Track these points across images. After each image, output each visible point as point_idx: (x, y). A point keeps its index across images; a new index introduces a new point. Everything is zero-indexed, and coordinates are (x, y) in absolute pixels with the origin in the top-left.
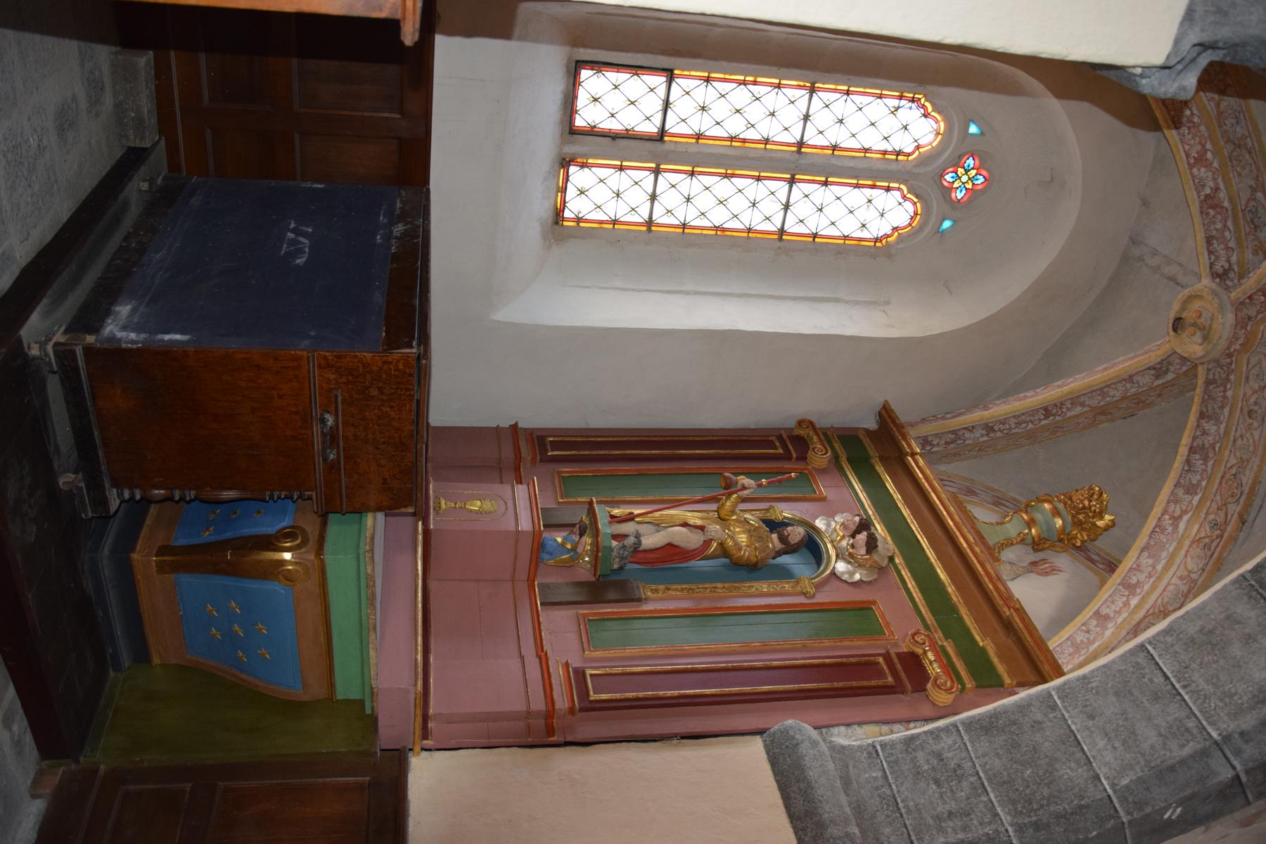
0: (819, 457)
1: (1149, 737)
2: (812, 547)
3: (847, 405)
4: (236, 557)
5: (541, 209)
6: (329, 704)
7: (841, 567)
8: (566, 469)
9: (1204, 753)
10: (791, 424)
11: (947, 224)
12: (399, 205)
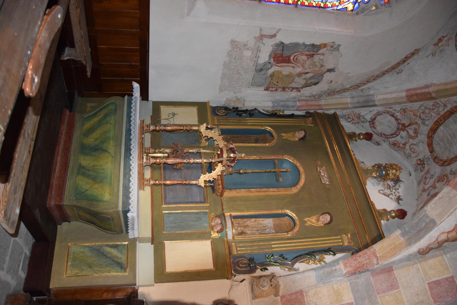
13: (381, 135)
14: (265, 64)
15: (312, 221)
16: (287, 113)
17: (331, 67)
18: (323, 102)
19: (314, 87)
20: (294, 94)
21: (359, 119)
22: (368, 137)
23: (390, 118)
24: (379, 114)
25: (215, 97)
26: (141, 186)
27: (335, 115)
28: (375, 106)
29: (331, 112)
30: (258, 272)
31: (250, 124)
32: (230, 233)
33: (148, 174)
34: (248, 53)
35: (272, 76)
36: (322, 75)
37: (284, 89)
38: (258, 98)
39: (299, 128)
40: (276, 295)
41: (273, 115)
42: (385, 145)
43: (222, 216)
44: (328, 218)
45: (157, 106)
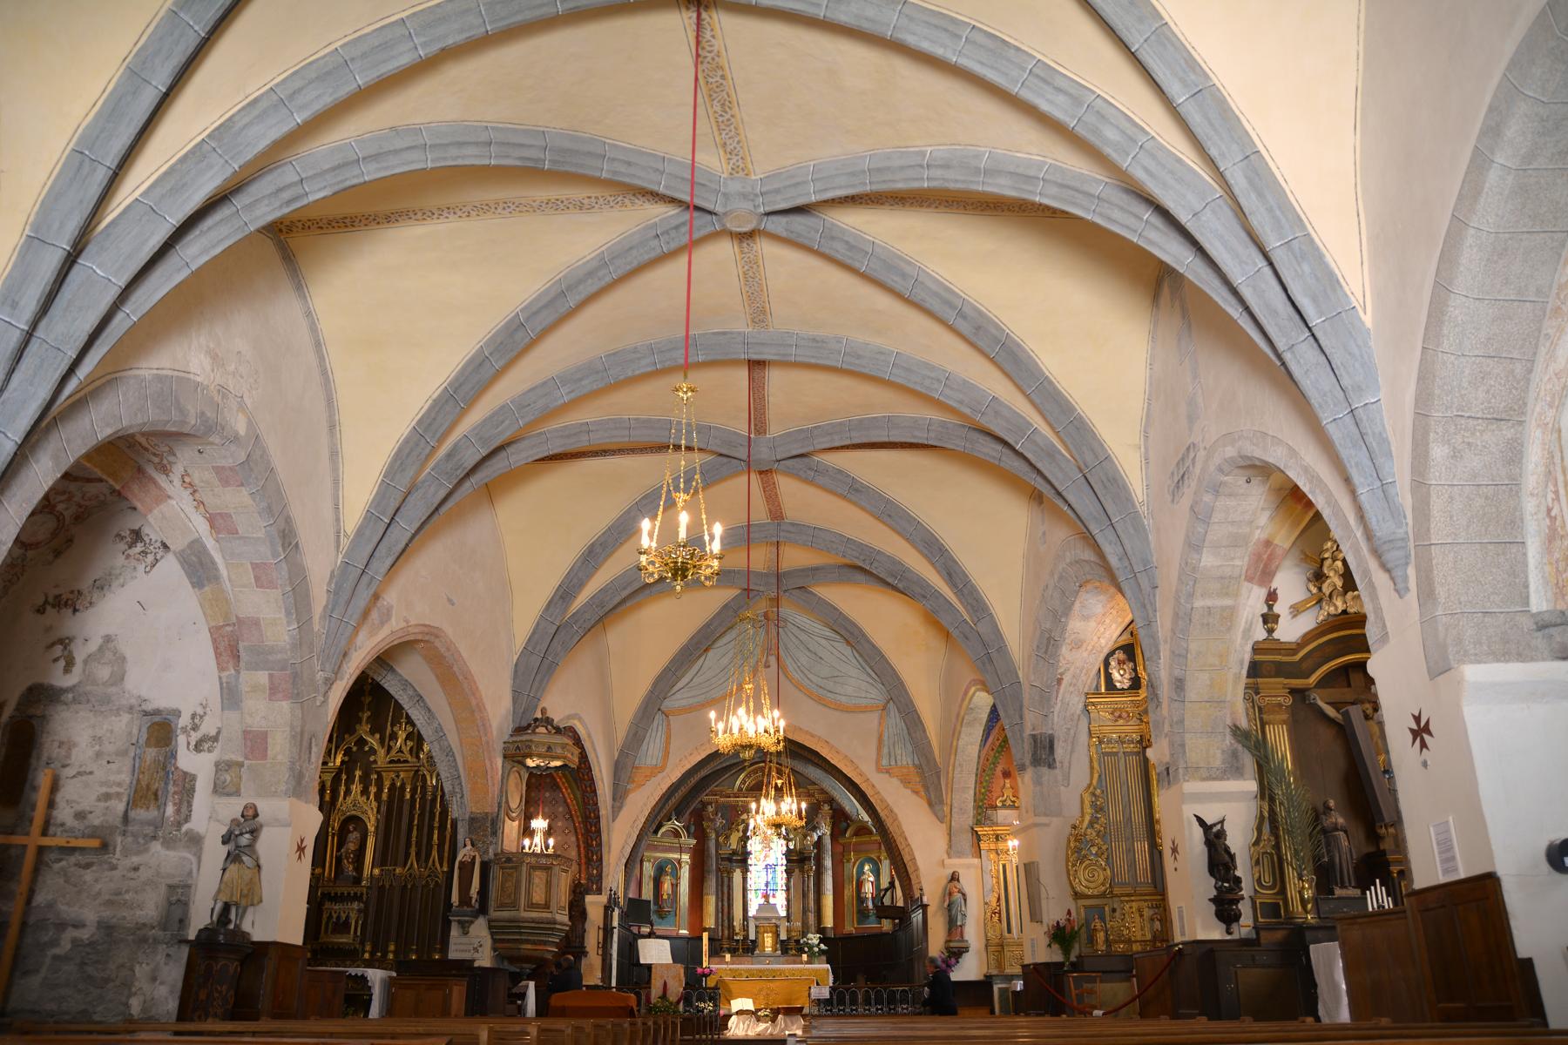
13: (54, 534)
40: (241, 765)
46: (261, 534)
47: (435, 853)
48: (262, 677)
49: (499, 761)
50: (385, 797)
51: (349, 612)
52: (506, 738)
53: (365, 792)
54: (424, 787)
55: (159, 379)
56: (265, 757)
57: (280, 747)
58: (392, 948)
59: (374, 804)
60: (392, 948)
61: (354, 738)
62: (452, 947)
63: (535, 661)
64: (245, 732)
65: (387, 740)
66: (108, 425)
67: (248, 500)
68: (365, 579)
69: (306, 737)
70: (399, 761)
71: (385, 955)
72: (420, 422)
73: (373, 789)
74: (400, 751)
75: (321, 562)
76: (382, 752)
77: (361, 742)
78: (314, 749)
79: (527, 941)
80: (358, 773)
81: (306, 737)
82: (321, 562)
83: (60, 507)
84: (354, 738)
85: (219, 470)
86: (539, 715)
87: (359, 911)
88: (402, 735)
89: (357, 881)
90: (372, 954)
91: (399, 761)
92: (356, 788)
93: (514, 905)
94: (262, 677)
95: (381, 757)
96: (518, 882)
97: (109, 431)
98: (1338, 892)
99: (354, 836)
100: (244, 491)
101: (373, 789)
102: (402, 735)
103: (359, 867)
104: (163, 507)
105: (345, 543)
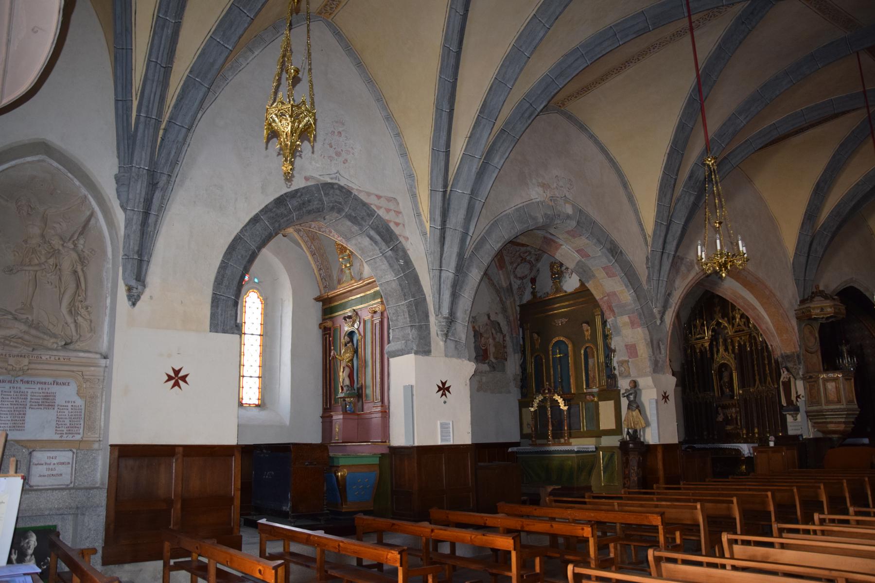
0: (329, 324)
1: (383, 267)
2: (351, 334)
3: (315, 312)
4: (342, 486)
5: (256, 411)
6: (380, 465)
7: (356, 326)
8: (333, 402)
9: (385, 257)
10: (321, 331)
11: (256, 280)
12: (742, 249)
13: (531, 270)
14: (489, 366)
15: (588, 334)
16: (521, 342)
17: (486, 317)
18: (512, 318)
19: (501, 325)
20: (508, 338)
21: (522, 289)
22: (533, 281)
23: (518, 269)
24: (516, 277)
25: (514, 397)
26: (570, 444)
27: (521, 306)
28: (510, 284)
29: (518, 308)
30: (616, 372)
31: (531, 369)
32: (595, 390)
33: (562, 440)
34: (484, 379)
35: (496, 358)
36: (492, 322)
37: (505, 347)
38: (513, 365)
39: (531, 337)
40: (627, 362)
41: (523, 352)
42: (539, 265)
43: (586, 394)
44: (584, 325)
45: (523, 436)
46: (600, 254)
47: (769, 379)
48: (626, 319)
49: (794, 322)
50: (736, 351)
51: (662, 274)
52: (796, 307)
53: (726, 350)
54: (756, 343)
55: (518, 210)
56: (637, 356)
57: (643, 351)
58: (756, 430)
59: (733, 355)
60: (756, 430)
61: (714, 322)
62: (789, 428)
63: (803, 260)
64: (626, 346)
65: (731, 321)
66: (498, 242)
67: (587, 241)
68: (665, 256)
69: (655, 343)
70: (740, 331)
71: (754, 434)
72: (665, 168)
73: (730, 347)
74: (739, 325)
75: (638, 255)
76: (729, 327)
77: (719, 324)
78: (662, 347)
79: (831, 423)
80: (721, 340)
81: (655, 343)
82: (638, 255)
83: (528, 258)
84: (714, 322)
85: (568, 232)
86: (814, 290)
87: (736, 412)
88: (738, 316)
89: (732, 397)
90: (747, 434)
91: (740, 331)
92: (721, 349)
93: (819, 403)
94: (626, 319)
95: (730, 331)
96: (819, 389)
97: (500, 245)
98: (612, 555)
99: (726, 374)
100: (583, 238)
101: (730, 347)
102: (738, 316)
103: (732, 390)
104: (559, 251)
105: (649, 240)
